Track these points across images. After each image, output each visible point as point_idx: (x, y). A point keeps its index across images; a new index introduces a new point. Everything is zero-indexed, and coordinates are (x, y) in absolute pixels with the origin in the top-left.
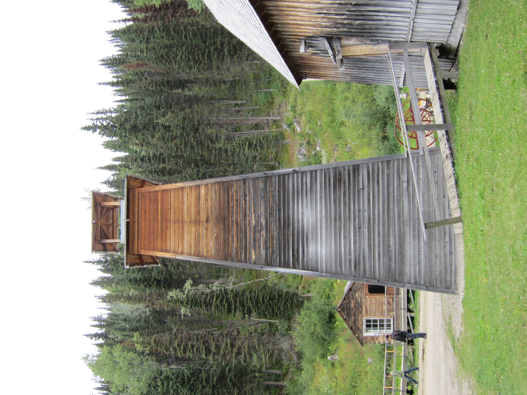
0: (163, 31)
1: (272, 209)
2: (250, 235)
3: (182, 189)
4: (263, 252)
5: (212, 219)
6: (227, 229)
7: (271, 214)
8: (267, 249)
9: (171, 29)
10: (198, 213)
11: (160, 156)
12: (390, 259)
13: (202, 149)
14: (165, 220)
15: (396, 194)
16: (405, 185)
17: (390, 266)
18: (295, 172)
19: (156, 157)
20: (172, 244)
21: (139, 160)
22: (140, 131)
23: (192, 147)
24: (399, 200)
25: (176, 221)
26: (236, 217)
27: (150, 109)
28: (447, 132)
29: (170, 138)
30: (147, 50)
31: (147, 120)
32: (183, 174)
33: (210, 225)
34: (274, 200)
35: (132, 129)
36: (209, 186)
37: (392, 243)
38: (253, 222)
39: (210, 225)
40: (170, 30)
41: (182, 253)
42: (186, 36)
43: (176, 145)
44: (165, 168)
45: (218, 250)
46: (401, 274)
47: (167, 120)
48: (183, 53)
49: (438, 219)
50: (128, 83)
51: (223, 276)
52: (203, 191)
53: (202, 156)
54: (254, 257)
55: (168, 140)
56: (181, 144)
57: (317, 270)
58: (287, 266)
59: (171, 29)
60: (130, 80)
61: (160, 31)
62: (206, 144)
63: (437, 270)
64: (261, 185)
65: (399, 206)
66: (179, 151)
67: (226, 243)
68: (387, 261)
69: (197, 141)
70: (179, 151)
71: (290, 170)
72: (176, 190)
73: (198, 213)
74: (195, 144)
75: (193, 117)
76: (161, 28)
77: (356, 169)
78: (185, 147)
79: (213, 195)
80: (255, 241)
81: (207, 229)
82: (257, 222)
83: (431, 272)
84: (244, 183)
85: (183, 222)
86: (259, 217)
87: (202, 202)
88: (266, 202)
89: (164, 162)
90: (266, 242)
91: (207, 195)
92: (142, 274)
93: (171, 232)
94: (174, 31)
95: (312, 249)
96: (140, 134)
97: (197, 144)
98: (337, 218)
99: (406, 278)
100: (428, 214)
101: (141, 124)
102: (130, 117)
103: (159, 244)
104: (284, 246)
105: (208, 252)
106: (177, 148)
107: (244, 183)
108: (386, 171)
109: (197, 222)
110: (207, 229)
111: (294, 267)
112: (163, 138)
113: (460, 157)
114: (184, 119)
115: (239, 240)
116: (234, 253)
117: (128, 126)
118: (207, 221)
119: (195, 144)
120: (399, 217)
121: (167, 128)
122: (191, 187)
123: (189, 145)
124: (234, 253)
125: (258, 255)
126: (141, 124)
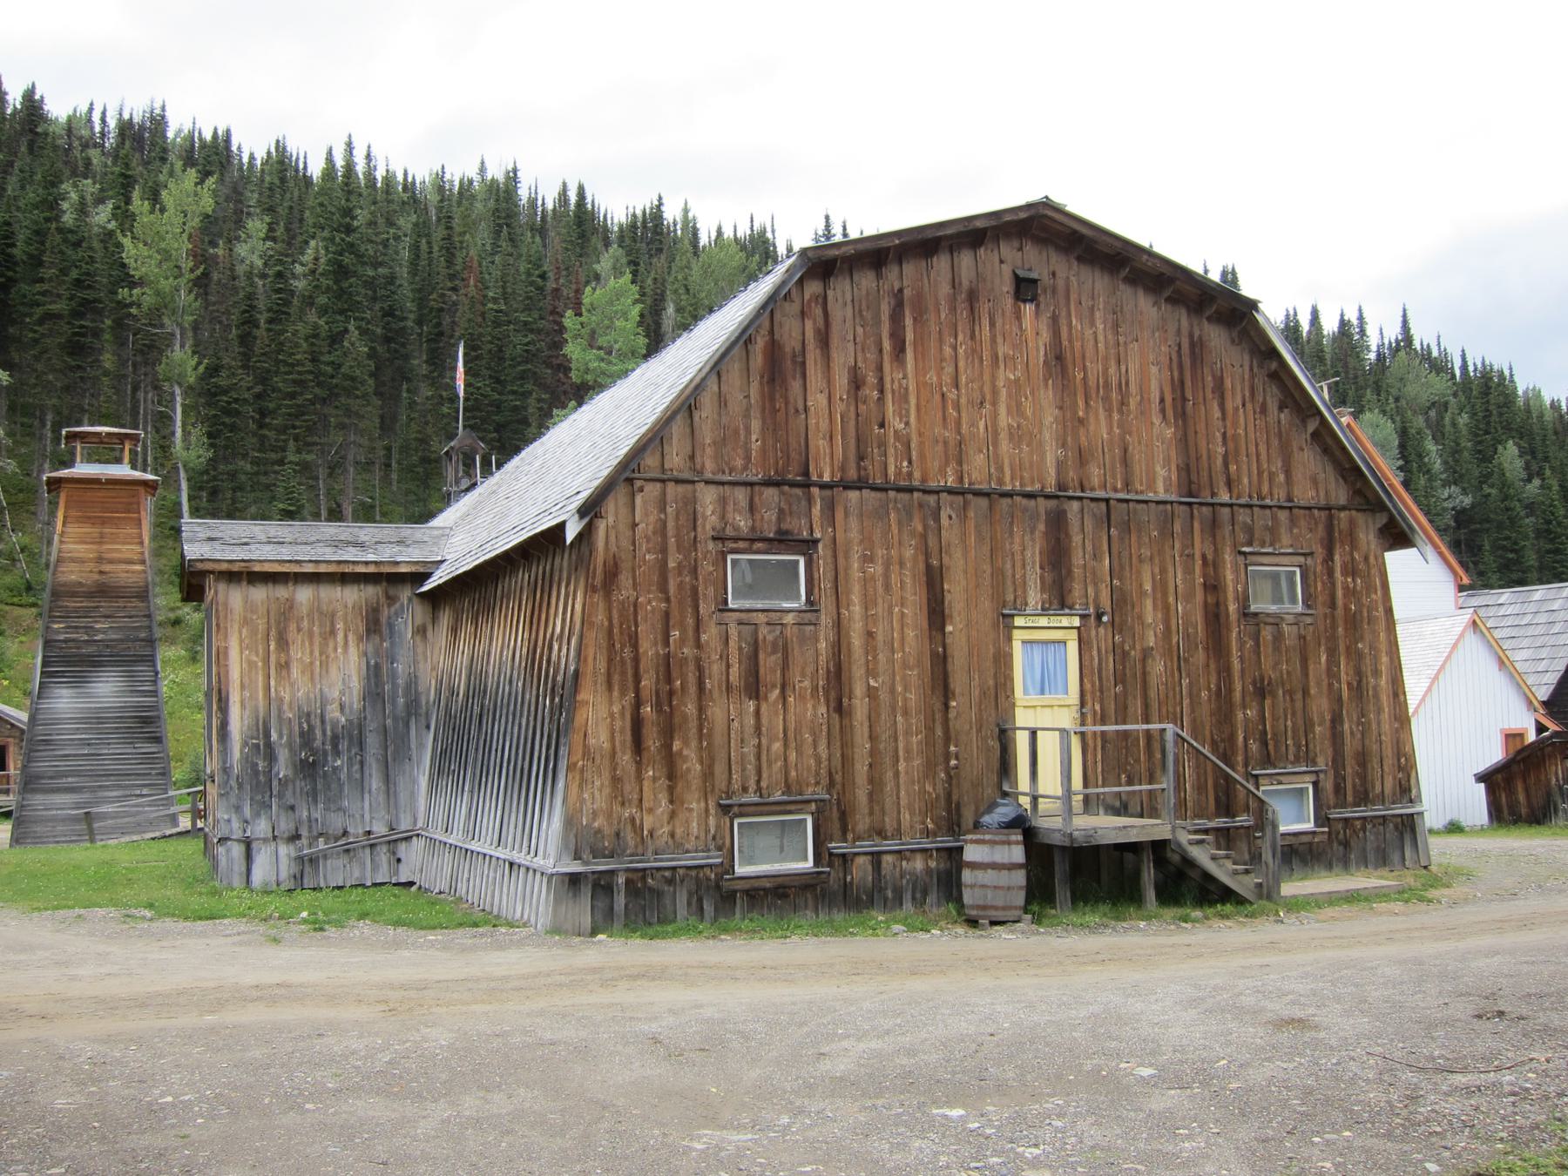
0: (526, 351)
1: (112, 647)
2: (83, 622)
3: (142, 543)
4: (62, 637)
5: (103, 578)
6: (90, 595)
7: (108, 646)
8: (65, 641)
9: (529, 366)
10: (111, 562)
11: (285, 313)
12: (51, 778)
13: (289, 415)
14: (104, 522)
15: (1100, 770)
16: (138, 792)
17: (43, 778)
18: (157, 673)
19: (284, 305)
20: (73, 529)
21: (278, 268)
22: (336, 282)
23: (292, 396)
24: (120, 786)
25: (102, 536)
26: (105, 606)
27: (388, 297)
28: (188, 832)
29: (315, 349)
30: (497, 311)
31: (358, 299)
32: (240, 371)
33: (96, 577)
34: (125, 649)
35: (340, 265)
36: (143, 575)
37: (70, 779)
38: (98, 626)
39: (96, 577)
40: (527, 362)
41: (61, 542)
42: (514, 392)
43: (299, 363)
44: (258, 327)
45: (65, 585)
46: (34, 791)
47: (353, 345)
48: (479, 388)
49: (96, 825)
50: (448, 249)
51: (15, 423)
52: (138, 567)
53: (273, 413)
54: (56, 626)
55: (313, 344)
56: (300, 373)
57: (39, 698)
58: (44, 664)
59: (529, 366)
60: (453, 255)
61: (526, 345)
62: (298, 423)
63: (38, 829)
64: (143, 635)
65: (114, 786)
66: (287, 369)
67: (74, 595)
68: (49, 774)
69: (303, 406)
70: (287, 369)
71: (159, 668)
72: (140, 536)
73: (111, 562)
74: (299, 401)
75: (357, 397)
76: (531, 347)
77: (158, 740)
78: (294, 382)
79: (133, 579)
80: (76, 627)
81: (91, 572)
82: (99, 631)
83: (35, 822)
84: (145, 616)
85: (100, 543)
86: (104, 633)
87: (124, 566)
88: (122, 640)
89: (270, 321)
90: (73, 640)
91: (133, 572)
92: (24, 262)
93: (87, 529)
94: (524, 371)
95: (65, 692)
96: (331, 283)
97: (298, 406)
98: (100, 720)
99: (29, 796)
100: (103, 817)
101: (351, 286)
102: (366, 263)
103: (73, 513)
104: (69, 661)
105: (63, 572)
106: (293, 365)
107: (145, 616)
108: (154, 772)
109: (100, 560)
110: (91, 572)
111: (42, 673)
112: (316, 336)
113: (162, 844)
114: (353, 379)
115: (76, 610)
116: (60, 603)
117: (347, 259)
118: (101, 572)
119: (299, 401)
120: (100, 787)
121: (336, 339)
122: (142, 553)
123: (298, 389)
124: (60, 603)
125: (58, 632)
126: (351, 286)
